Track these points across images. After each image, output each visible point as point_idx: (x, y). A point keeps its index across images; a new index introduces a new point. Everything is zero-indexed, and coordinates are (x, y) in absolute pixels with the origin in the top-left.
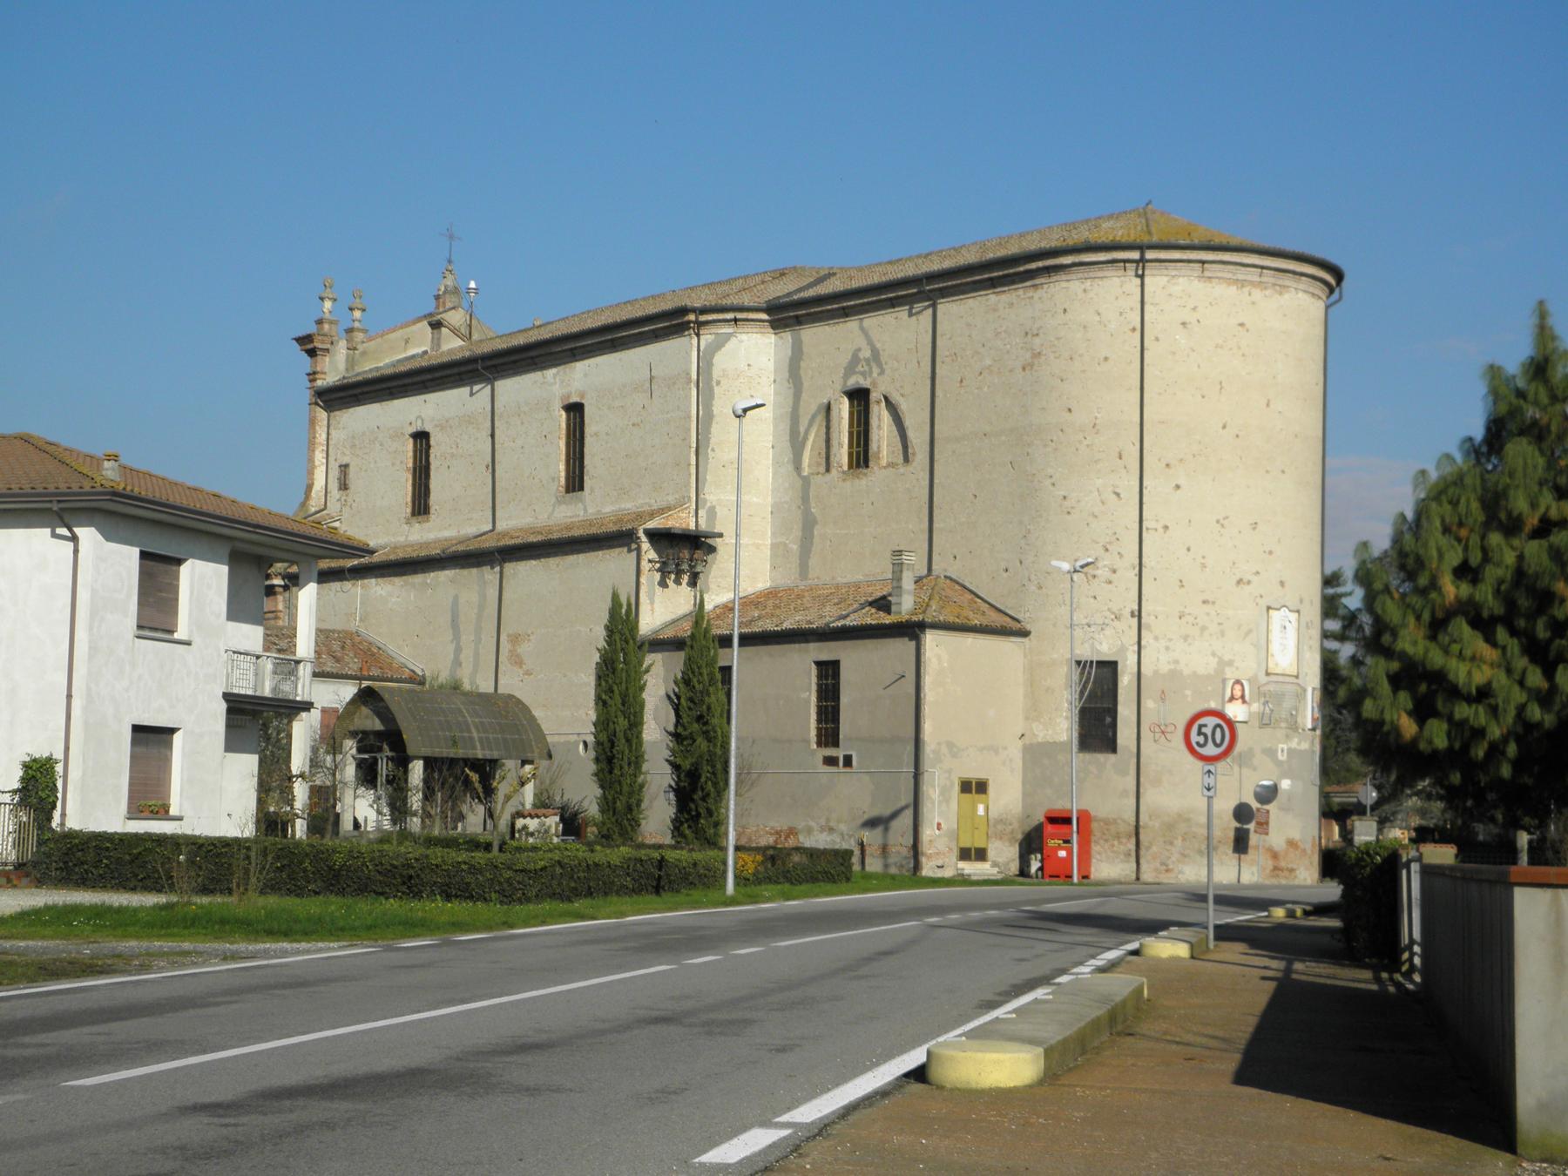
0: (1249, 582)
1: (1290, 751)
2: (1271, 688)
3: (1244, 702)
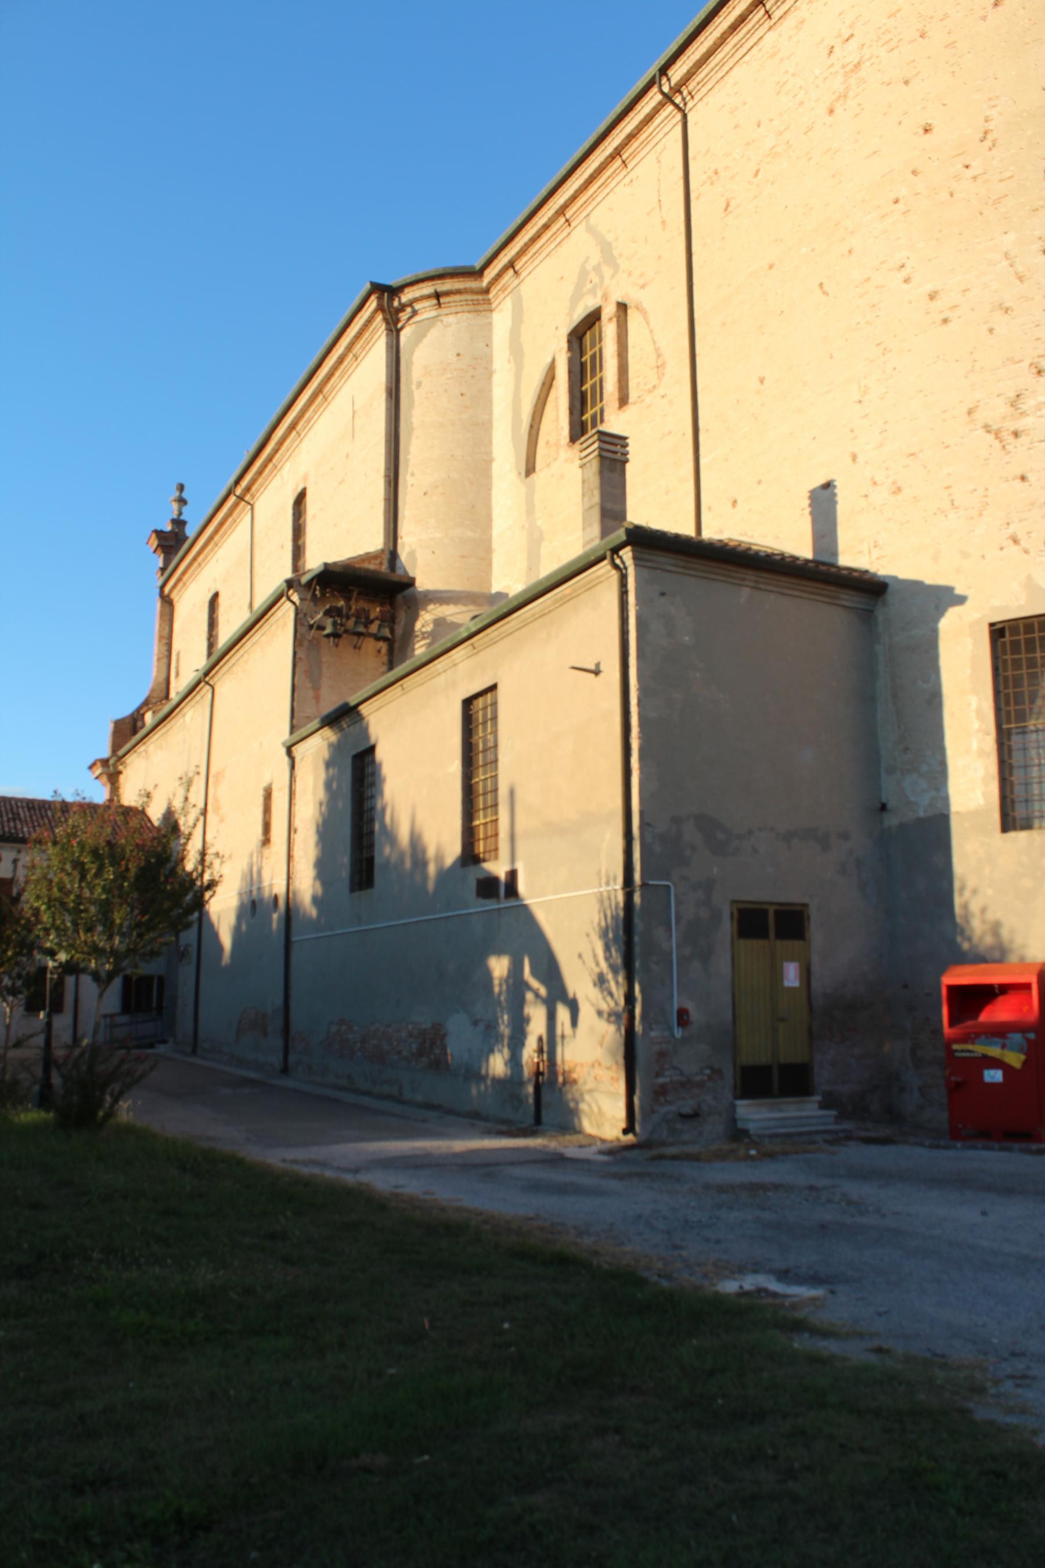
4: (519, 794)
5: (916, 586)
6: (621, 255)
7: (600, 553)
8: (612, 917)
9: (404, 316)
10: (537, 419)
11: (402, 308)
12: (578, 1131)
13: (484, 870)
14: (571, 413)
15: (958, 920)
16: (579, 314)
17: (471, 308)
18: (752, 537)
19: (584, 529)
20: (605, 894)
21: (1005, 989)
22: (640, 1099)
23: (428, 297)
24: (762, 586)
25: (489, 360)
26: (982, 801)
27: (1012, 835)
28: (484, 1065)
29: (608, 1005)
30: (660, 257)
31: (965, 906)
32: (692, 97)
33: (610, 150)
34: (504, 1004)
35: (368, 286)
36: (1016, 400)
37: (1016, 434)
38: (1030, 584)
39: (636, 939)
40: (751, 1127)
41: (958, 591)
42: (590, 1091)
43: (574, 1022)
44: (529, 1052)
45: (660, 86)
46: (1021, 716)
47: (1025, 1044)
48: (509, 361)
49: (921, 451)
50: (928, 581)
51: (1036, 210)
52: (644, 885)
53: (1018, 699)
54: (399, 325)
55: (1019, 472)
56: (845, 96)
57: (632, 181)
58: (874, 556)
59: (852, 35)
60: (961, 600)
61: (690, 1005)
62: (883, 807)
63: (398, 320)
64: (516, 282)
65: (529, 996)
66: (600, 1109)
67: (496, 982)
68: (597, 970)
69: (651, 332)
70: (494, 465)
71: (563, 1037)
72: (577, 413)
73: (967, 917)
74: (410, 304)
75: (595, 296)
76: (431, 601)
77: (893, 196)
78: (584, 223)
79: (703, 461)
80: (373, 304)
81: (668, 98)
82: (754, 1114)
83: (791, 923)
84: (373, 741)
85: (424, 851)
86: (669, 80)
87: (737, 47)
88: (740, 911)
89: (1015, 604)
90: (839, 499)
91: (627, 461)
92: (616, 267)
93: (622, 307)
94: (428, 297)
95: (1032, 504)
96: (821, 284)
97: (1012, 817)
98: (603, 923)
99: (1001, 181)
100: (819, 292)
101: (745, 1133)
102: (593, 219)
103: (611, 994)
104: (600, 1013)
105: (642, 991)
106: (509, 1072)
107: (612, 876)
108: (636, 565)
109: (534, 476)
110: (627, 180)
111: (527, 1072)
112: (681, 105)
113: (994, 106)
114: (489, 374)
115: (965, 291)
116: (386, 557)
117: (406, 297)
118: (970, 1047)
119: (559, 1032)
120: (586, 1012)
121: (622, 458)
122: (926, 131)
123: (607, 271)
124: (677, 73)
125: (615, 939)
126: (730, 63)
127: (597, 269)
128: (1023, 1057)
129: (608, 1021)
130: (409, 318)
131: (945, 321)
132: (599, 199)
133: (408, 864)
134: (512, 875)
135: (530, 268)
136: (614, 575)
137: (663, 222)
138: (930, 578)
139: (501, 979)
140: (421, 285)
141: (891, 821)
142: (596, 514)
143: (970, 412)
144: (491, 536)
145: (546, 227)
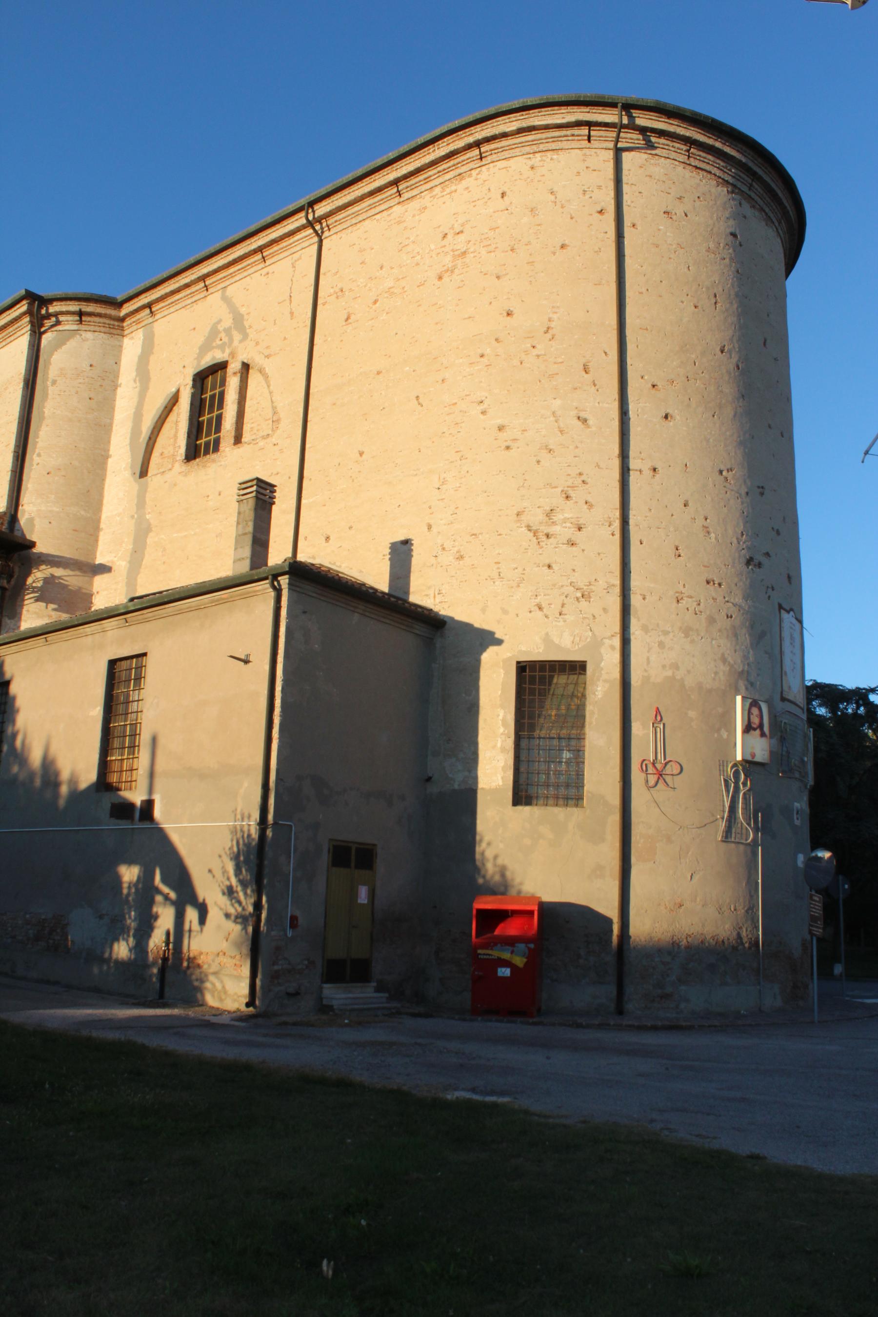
3: (763, 735)
4: (161, 742)
6: (250, 327)
8: (244, 844)
9: (48, 323)
10: (156, 433)
11: (48, 316)
12: (203, 1004)
13: (120, 797)
14: (189, 436)
15: (478, 863)
16: (207, 361)
18: (340, 567)
19: (236, 549)
20: (238, 827)
21: (515, 913)
22: (262, 981)
24: (367, 614)
26: (501, 783)
27: (519, 808)
28: (108, 950)
29: (236, 910)
30: (285, 339)
31: (483, 854)
32: (329, 230)
33: (254, 246)
34: (132, 903)
35: (23, 292)
37: (548, 536)
38: (547, 639)
39: (266, 862)
40: (335, 1003)
41: (498, 635)
42: (215, 973)
43: (202, 920)
44: (157, 940)
46: (532, 727)
47: (527, 951)
48: (135, 381)
49: (481, 534)
50: (477, 625)
52: (275, 823)
53: (532, 717)
54: (43, 329)
55: (547, 562)
56: (452, 272)
57: (268, 274)
58: (437, 600)
59: (462, 232)
60: (499, 642)
61: (297, 913)
63: (42, 325)
64: (151, 320)
65: (159, 898)
66: (224, 987)
67: (125, 885)
69: (271, 393)
70: (110, 461)
71: (190, 931)
72: (193, 437)
73: (484, 860)
74: (56, 315)
75: (223, 352)
76: (43, 562)
77: (480, 351)
78: (220, 292)
79: (303, 501)
80: (23, 307)
81: (310, 224)
82: (336, 995)
84: (8, 676)
85: (57, 774)
86: (314, 212)
87: (371, 207)
88: (335, 847)
90: (414, 553)
91: (274, 503)
92: (245, 336)
93: (246, 367)
95: (554, 585)
96: (417, 397)
97: (521, 796)
98: (235, 849)
99: (555, 363)
100: (416, 402)
101: (330, 1008)
102: (230, 291)
103: (240, 903)
104: (227, 916)
105: (268, 901)
107: (246, 814)
108: (289, 589)
113: (556, 313)
114: (115, 387)
115: (524, 431)
116: (7, 519)
117: (52, 309)
118: (490, 952)
119: (187, 927)
120: (214, 915)
121: (270, 500)
122: (508, 314)
123: (237, 337)
124: (321, 209)
125: (247, 861)
126: (364, 216)
127: (228, 331)
128: (525, 960)
129: (235, 922)
130: (52, 326)
131: (508, 448)
132: (237, 278)
133: (38, 782)
134: (149, 805)
135: (166, 313)
137: (292, 313)
138: (479, 622)
139: (130, 883)
140: (68, 303)
141: (433, 789)
142: (249, 540)
144: (100, 517)
145: (187, 286)
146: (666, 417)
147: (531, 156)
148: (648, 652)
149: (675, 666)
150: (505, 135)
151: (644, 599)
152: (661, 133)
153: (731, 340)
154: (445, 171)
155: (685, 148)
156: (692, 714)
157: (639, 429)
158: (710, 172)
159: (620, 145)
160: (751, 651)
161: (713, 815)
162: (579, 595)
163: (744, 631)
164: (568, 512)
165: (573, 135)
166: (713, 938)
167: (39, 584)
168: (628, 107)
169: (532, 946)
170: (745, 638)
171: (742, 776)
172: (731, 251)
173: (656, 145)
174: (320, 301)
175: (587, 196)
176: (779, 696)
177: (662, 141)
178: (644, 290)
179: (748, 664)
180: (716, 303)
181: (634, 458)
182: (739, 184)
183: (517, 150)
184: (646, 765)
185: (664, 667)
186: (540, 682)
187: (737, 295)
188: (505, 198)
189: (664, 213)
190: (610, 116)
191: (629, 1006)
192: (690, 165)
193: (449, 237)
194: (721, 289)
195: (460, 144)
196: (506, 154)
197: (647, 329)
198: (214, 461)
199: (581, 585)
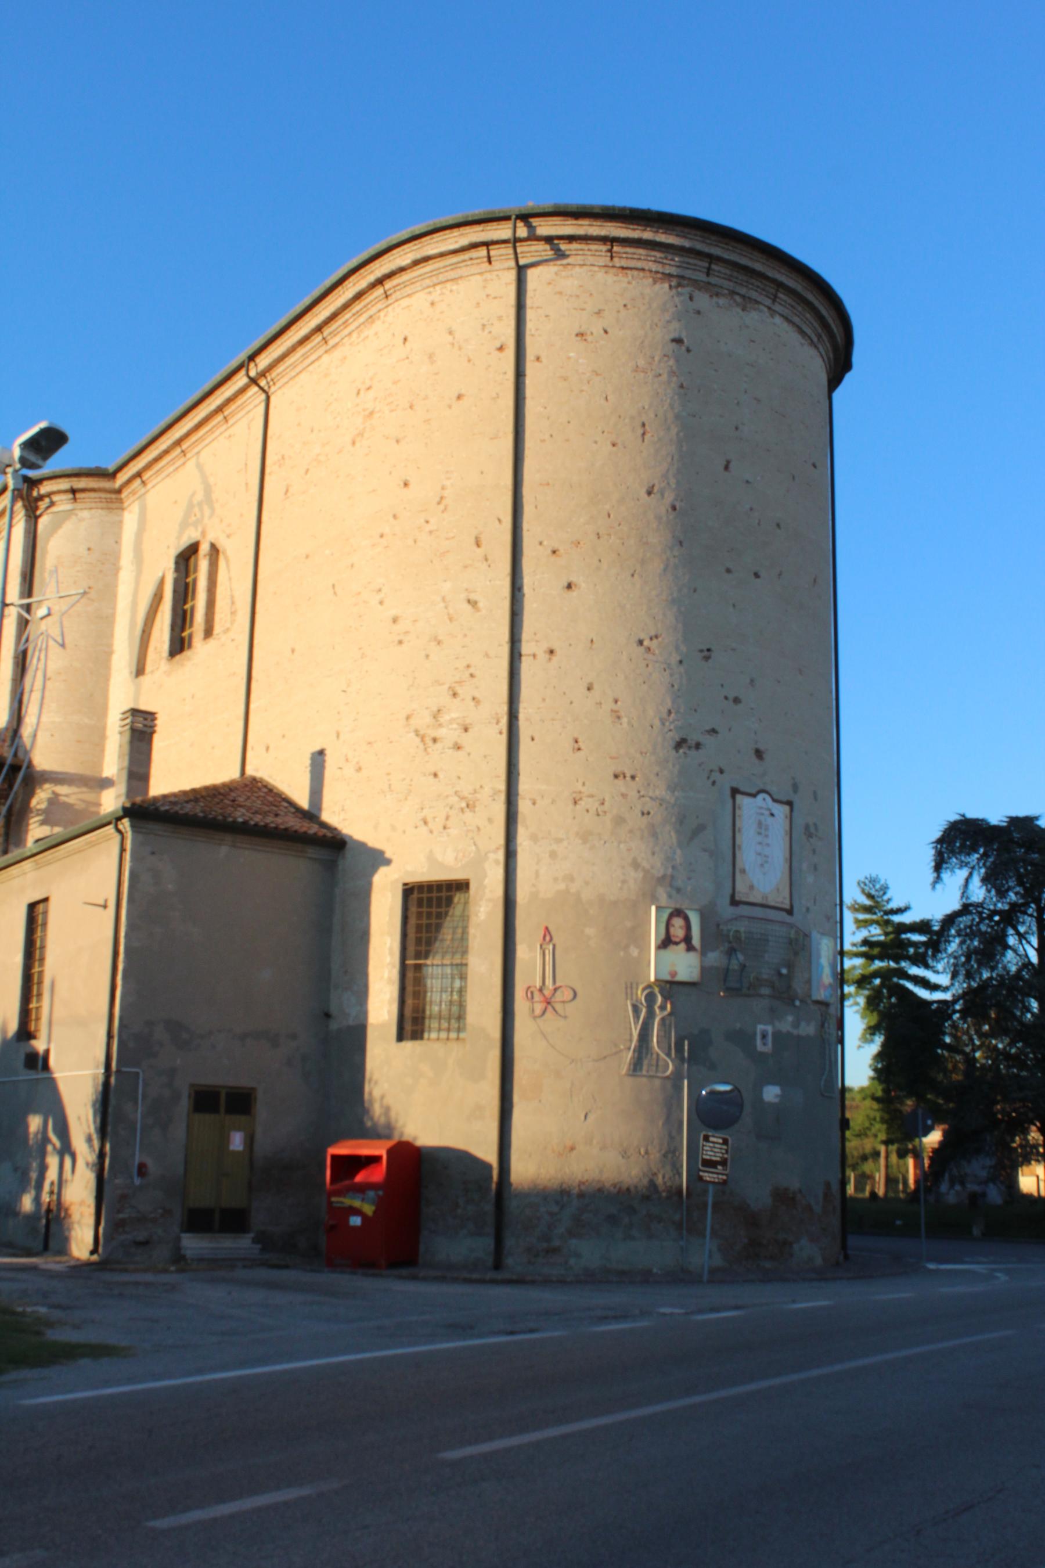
0: (698, 746)
1: (777, 1035)
2: (742, 927)
3: (690, 948)
5: (362, 846)
7: (108, 820)
9: (43, 505)
11: (41, 498)
13: (32, 1047)
15: (366, 1105)
16: (184, 543)
17: (104, 505)
22: (105, 1229)
23: (65, 491)
25: (117, 556)
27: (404, 1044)
31: (370, 1093)
36: (437, 714)
37: (435, 740)
38: (431, 858)
40: (189, 1254)
41: (388, 855)
45: (248, 370)
51: (466, 567)
52: (118, 1071)
54: (38, 513)
55: (433, 770)
60: (388, 862)
61: (149, 1162)
62: (327, 1015)
63: (37, 508)
65: (50, 1148)
68: (87, 1131)
72: (178, 629)
73: (371, 1101)
74: (49, 495)
79: (252, 706)
81: (254, 381)
82: (193, 1244)
83: (240, 1102)
86: (256, 365)
87: (305, 356)
89: (422, 872)
91: (154, 732)
94: (65, 491)
99: (447, 539)
102: (203, 454)
105: (112, 1149)
106: (33, 1209)
108: (133, 831)
109: (141, 678)
110: (227, 434)
111: (44, 1208)
112: (266, 388)
114: (116, 570)
116: (10, 734)
117: (45, 488)
123: (207, 511)
124: (263, 361)
127: (200, 504)
128: (373, 1208)
132: (207, 441)
134: (47, 1052)
136: (117, 838)
141: (334, 1026)
143: (408, 718)
145: (166, 452)
146: (569, 586)
147: (431, 289)
148: (537, 863)
149: (570, 878)
150: (402, 270)
151: (534, 804)
152: (571, 239)
153: (665, 476)
154: (359, 313)
155: (604, 248)
156: (590, 931)
157: (535, 605)
158: (643, 270)
159: (522, 262)
160: (679, 852)
161: (616, 1045)
162: (464, 805)
163: (668, 827)
164: (455, 712)
165: (471, 259)
166: (615, 1185)
167: (43, 806)
168: (525, 217)
169: (381, 1193)
170: (669, 836)
171: (659, 999)
172: (671, 362)
173: (567, 253)
174: (268, 470)
175: (487, 331)
176: (728, 900)
177: (575, 246)
178: (547, 437)
179: (673, 867)
180: (644, 434)
181: (528, 641)
182: (688, 273)
183: (418, 284)
184: (532, 993)
185: (556, 879)
186: (431, 905)
187: (677, 417)
188: (407, 343)
189: (577, 335)
190: (503, 231)
191: (509, 1261)
192: (613, 267)
193: (362, 392)
194: (652, 416)
195: (363, 284)
196: (408, 290)
197: (548, 484)
198: (189, 659)
199: (466, 794)
